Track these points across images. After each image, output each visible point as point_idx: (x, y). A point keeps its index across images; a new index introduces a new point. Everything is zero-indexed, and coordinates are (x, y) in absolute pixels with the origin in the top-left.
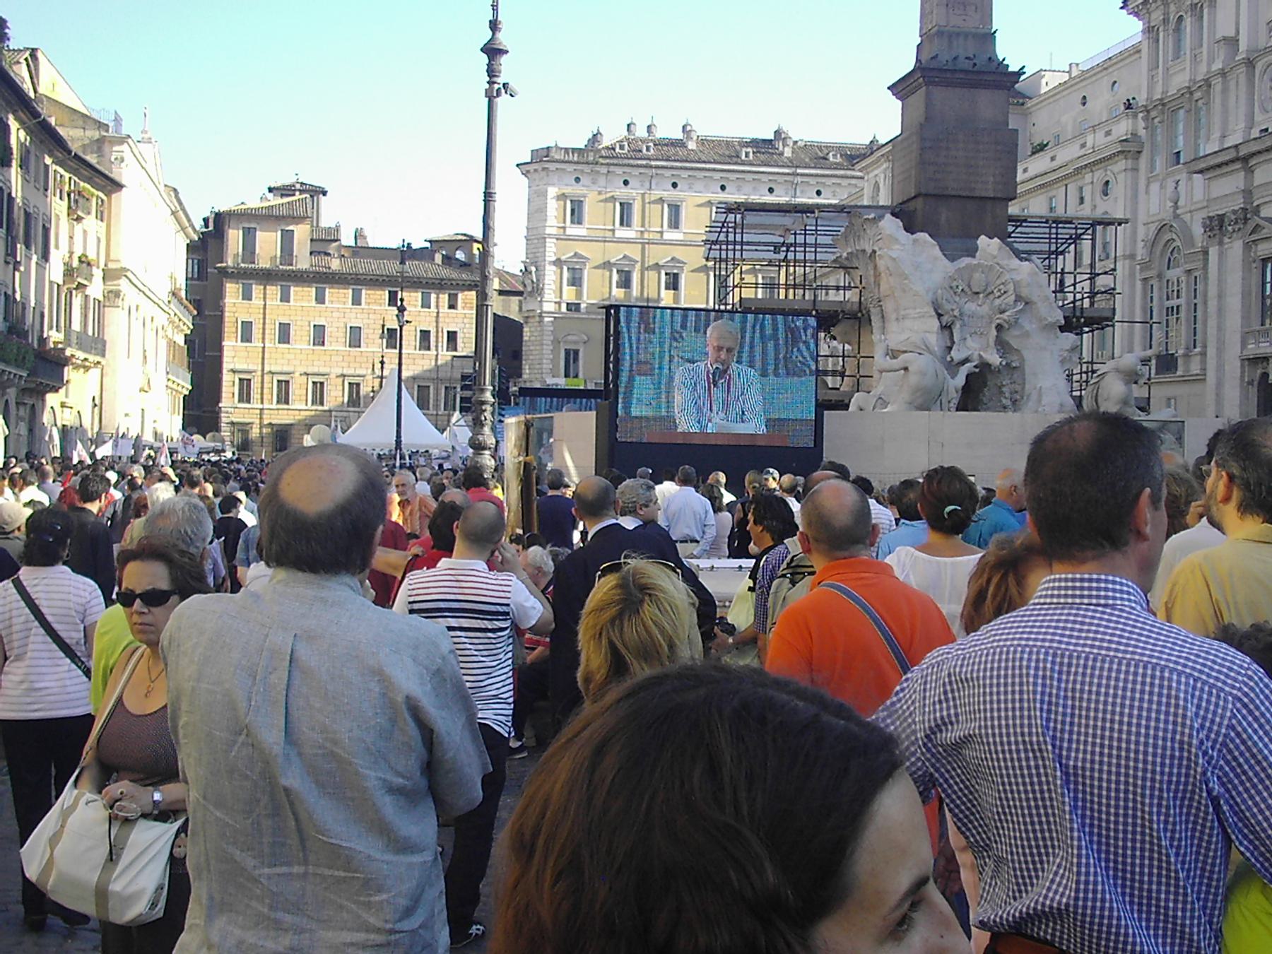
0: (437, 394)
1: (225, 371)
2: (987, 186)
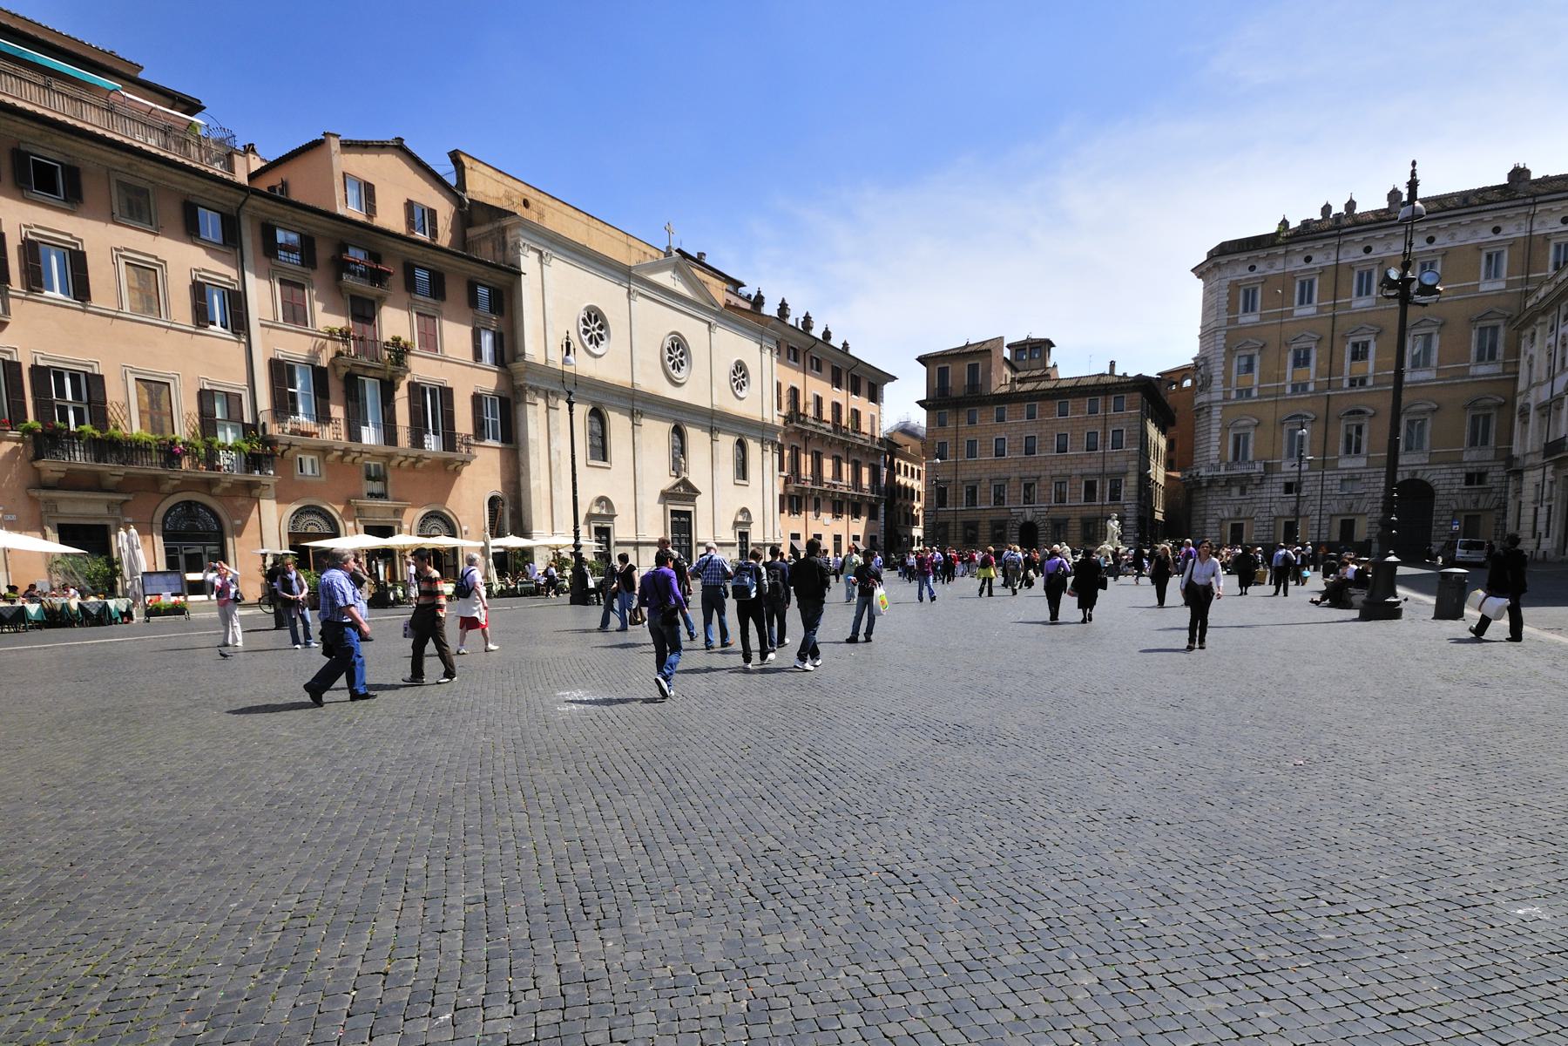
0: (1103, 488)
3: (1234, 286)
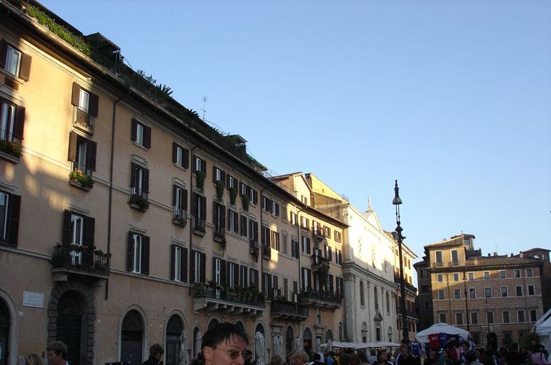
0: (527, 314)
1: (434, 312)
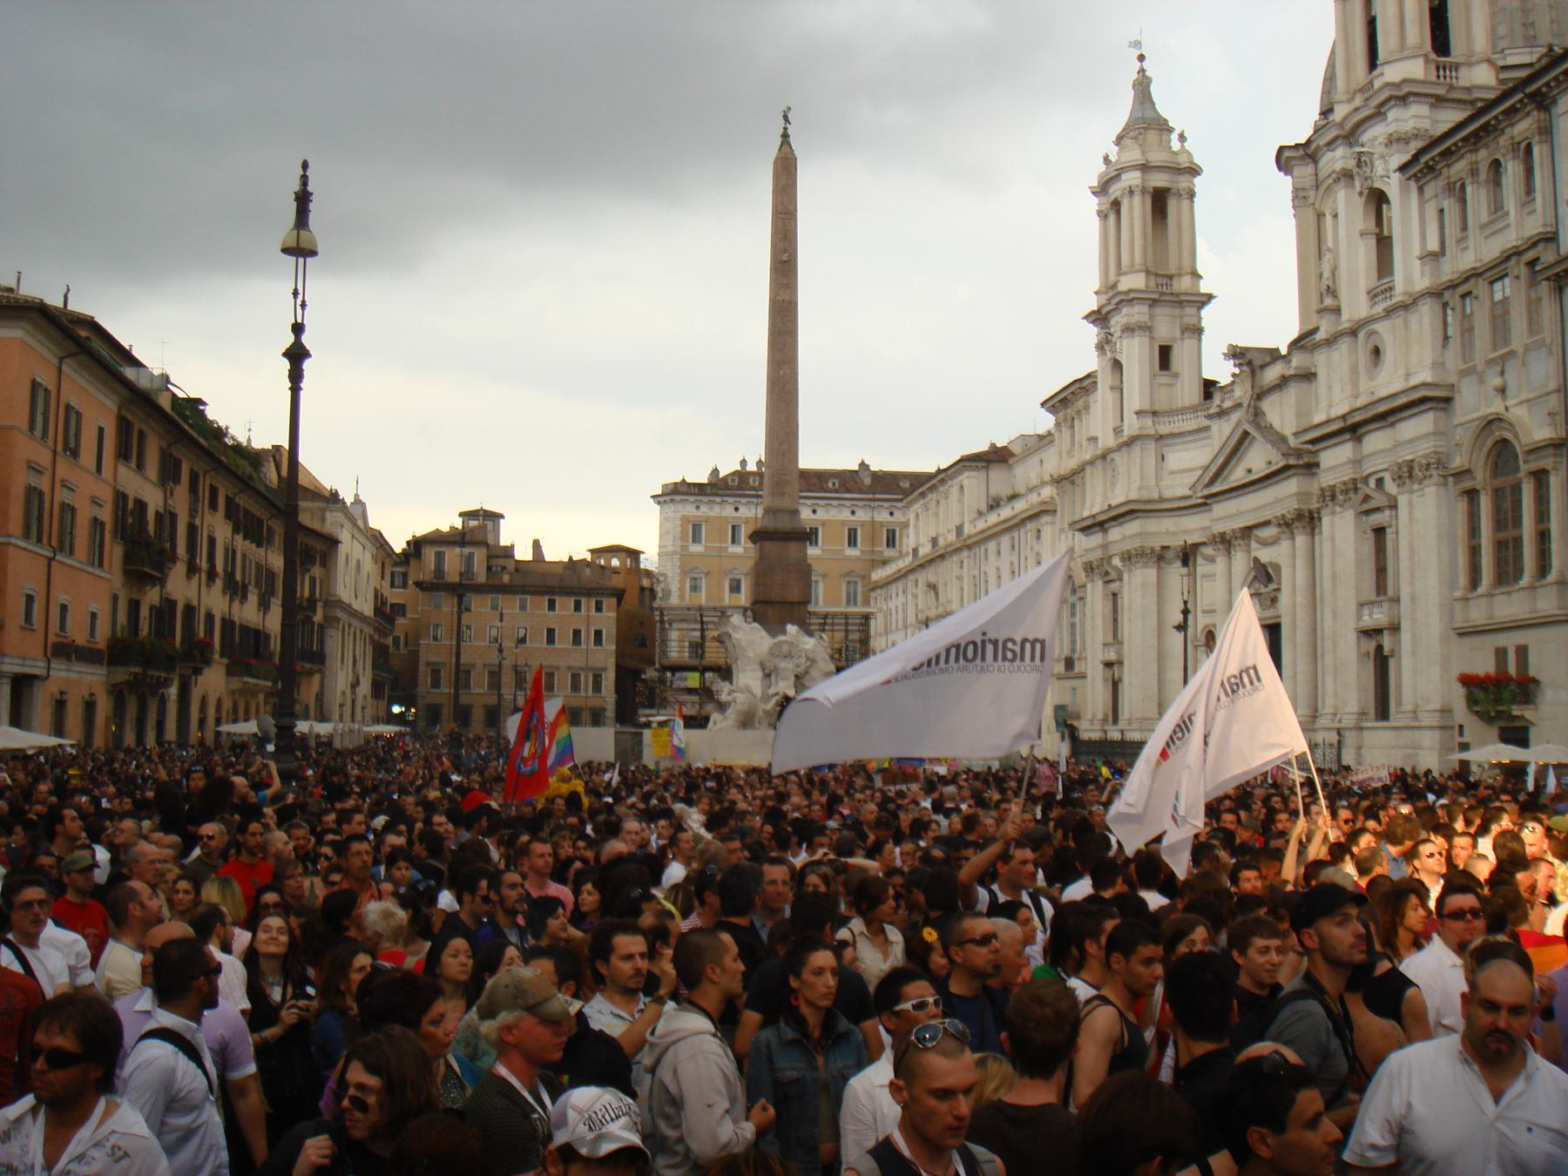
2: (794, 595)
3: (685, 519)
